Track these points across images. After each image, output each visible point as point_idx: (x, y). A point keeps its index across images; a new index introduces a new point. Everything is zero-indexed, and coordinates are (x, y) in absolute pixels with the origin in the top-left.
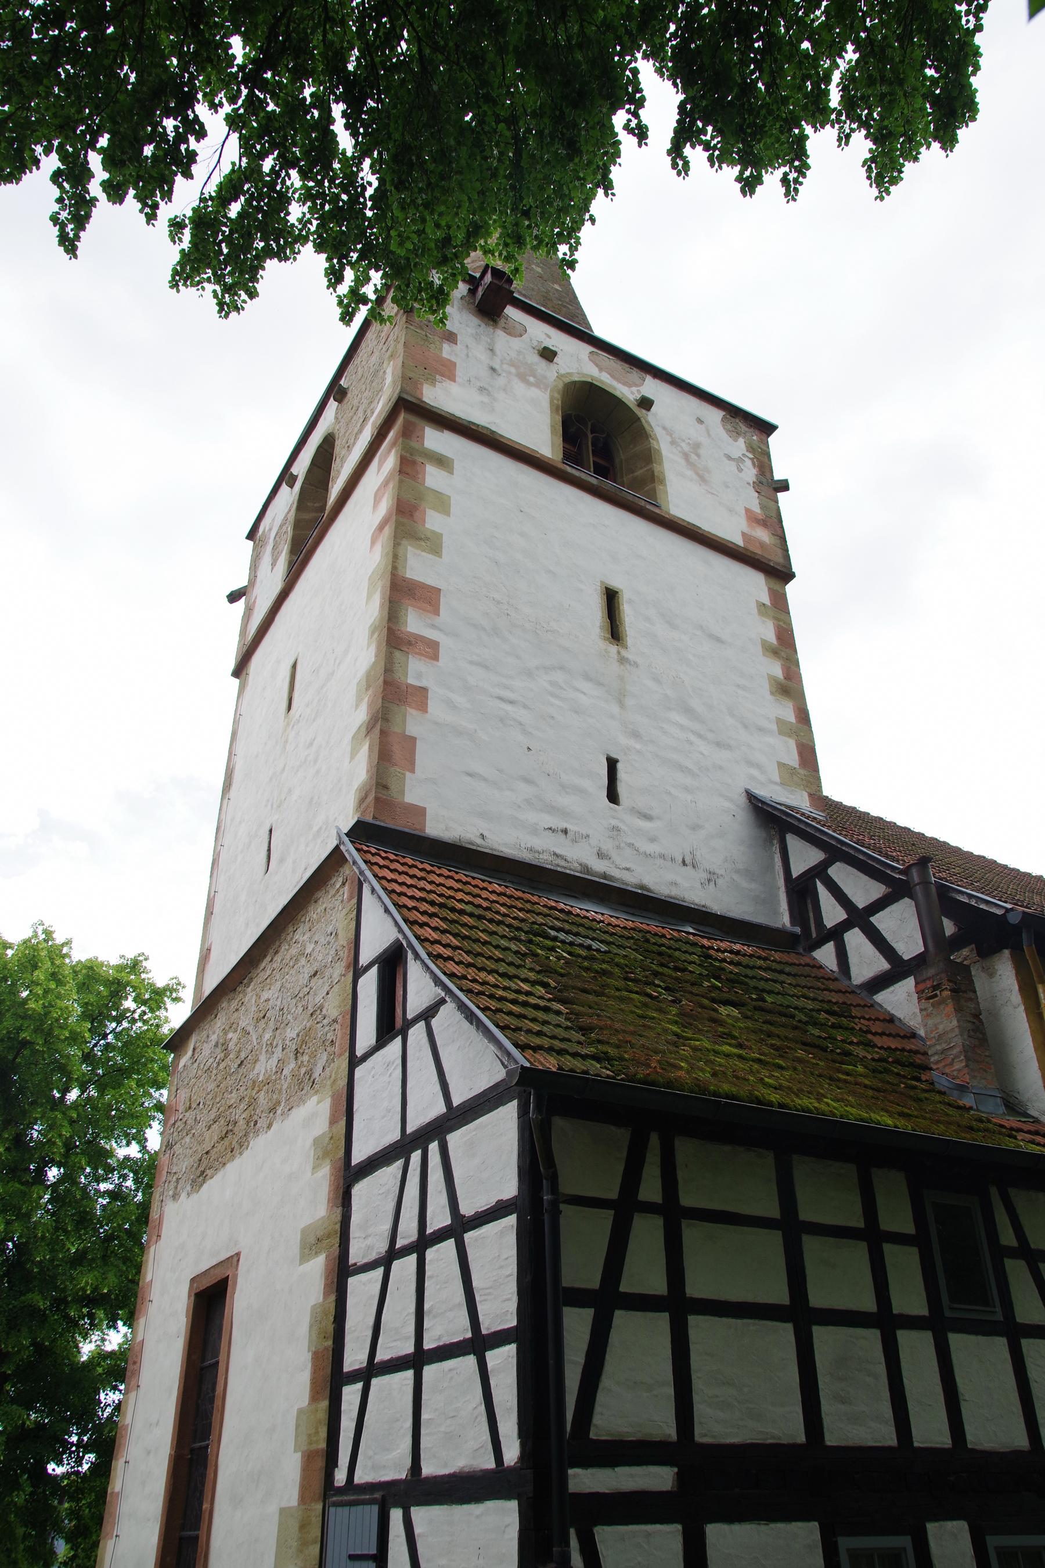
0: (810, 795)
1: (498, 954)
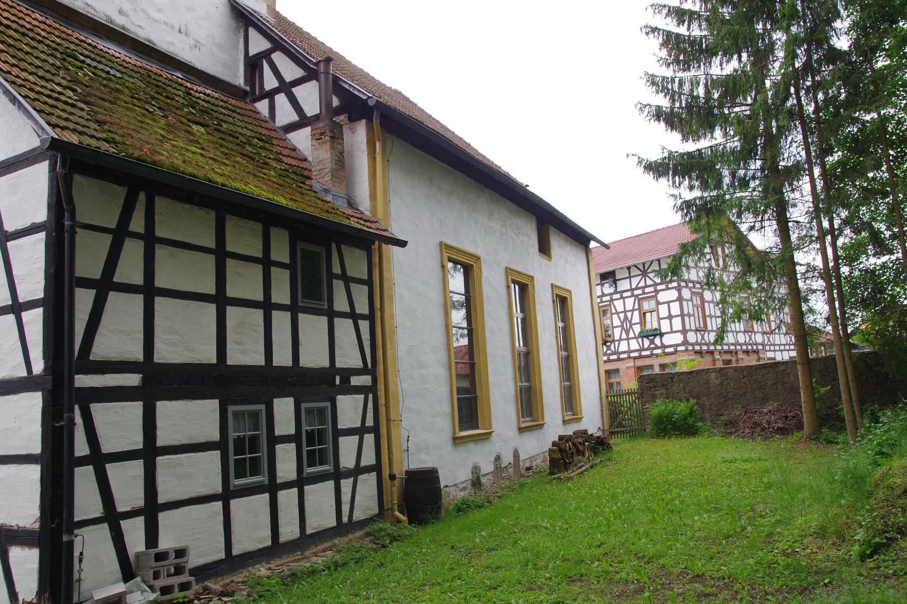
0: (268, 6)
1: (37, 62)
